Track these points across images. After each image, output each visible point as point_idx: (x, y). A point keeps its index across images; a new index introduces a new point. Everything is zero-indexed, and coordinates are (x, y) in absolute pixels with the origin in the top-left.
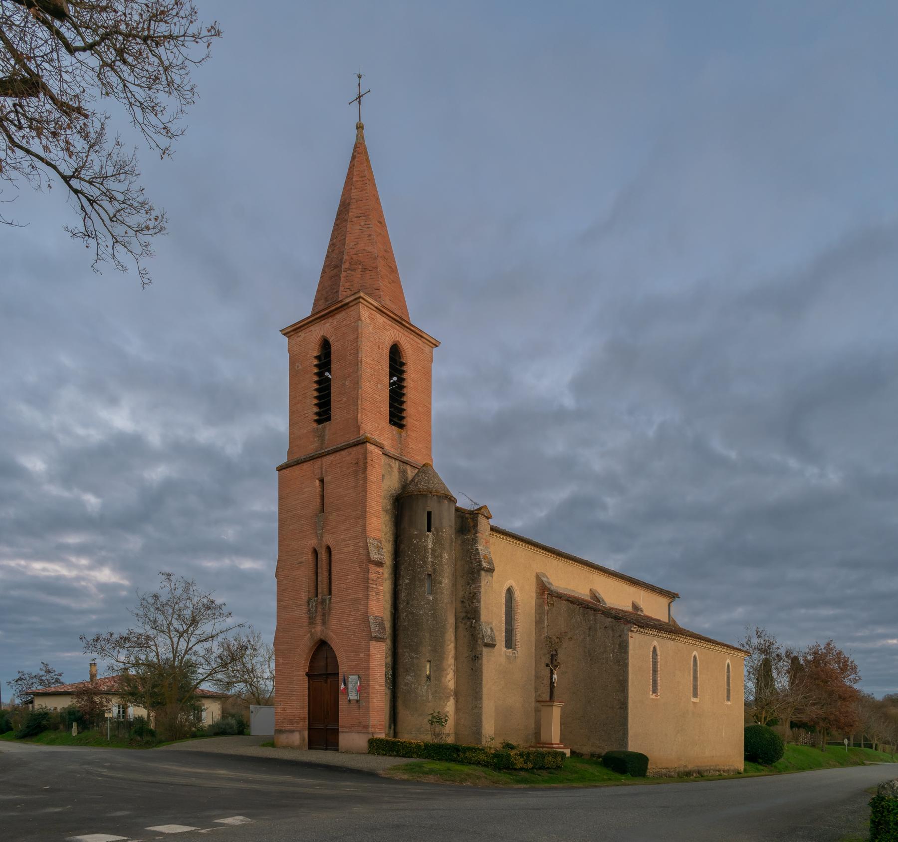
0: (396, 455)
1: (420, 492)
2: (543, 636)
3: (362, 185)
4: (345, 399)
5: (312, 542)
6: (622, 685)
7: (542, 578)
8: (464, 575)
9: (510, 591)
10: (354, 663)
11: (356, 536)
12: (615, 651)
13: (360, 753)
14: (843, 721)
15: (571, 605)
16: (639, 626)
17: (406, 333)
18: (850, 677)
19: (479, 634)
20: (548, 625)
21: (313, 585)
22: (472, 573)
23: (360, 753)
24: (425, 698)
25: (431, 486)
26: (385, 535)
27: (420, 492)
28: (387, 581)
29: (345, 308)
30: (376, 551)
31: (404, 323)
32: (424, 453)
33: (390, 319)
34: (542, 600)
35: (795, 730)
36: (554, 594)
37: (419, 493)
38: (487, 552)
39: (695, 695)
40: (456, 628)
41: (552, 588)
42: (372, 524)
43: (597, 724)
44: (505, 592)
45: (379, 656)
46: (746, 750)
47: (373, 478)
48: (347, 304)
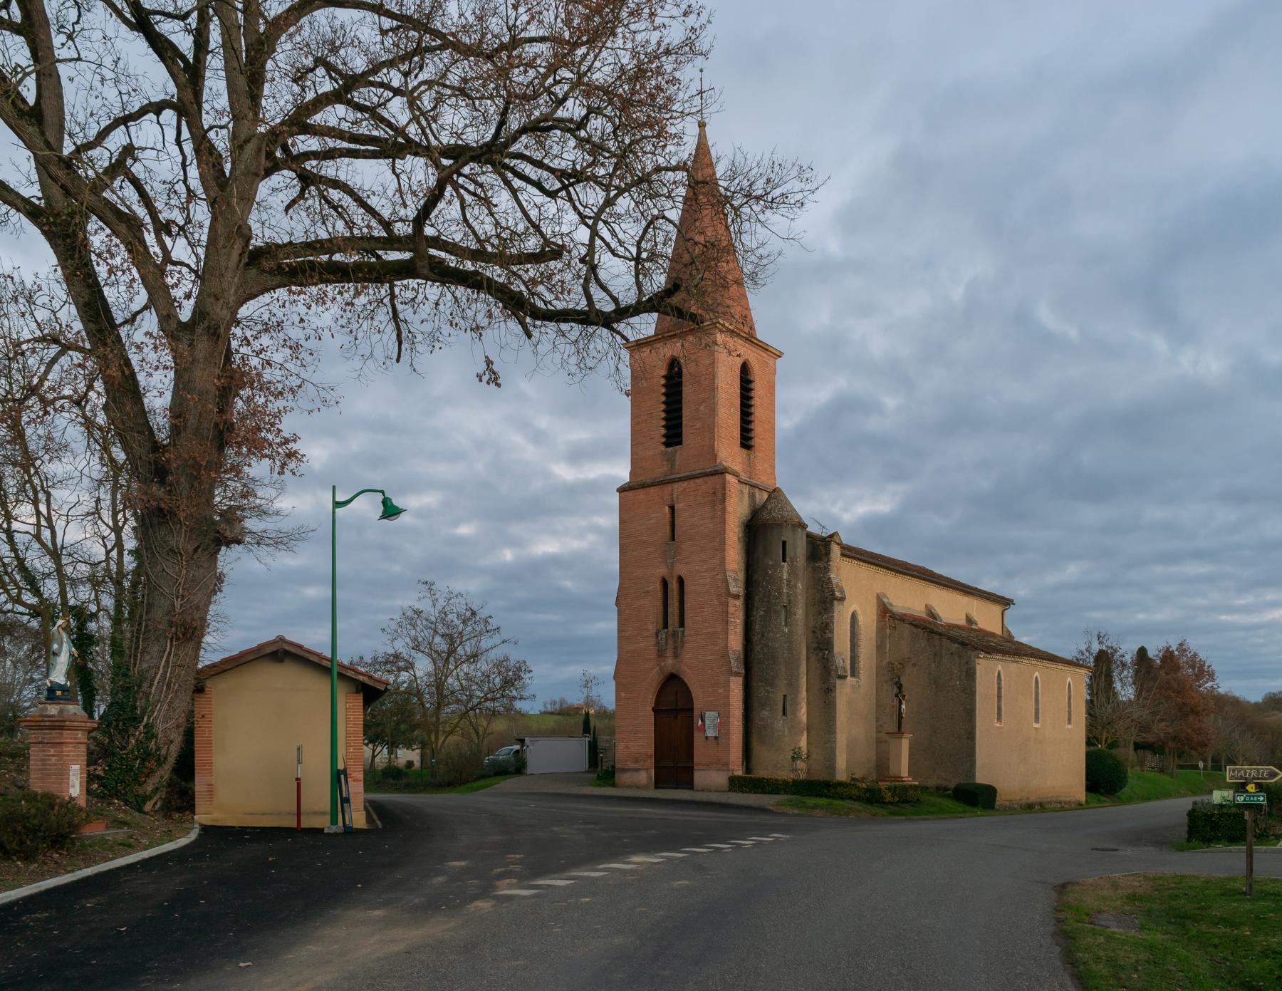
2: (885, 662)
4: (699, 425)
5: (662, 571)
6: (969, 713)
9: (854, 616)
10: (711, 699)
11: (714, 569)
14: (1196, 739)
16: (986, 652)
18: (1207, 685)
20: (890, 650)
21: (661, 615)
22: (825, 602)
25: (786, 514)
35: (1141, 752)
39: (1037, 720)
40: (808, 658)
41: (894, 610)
46: (1087, 779)
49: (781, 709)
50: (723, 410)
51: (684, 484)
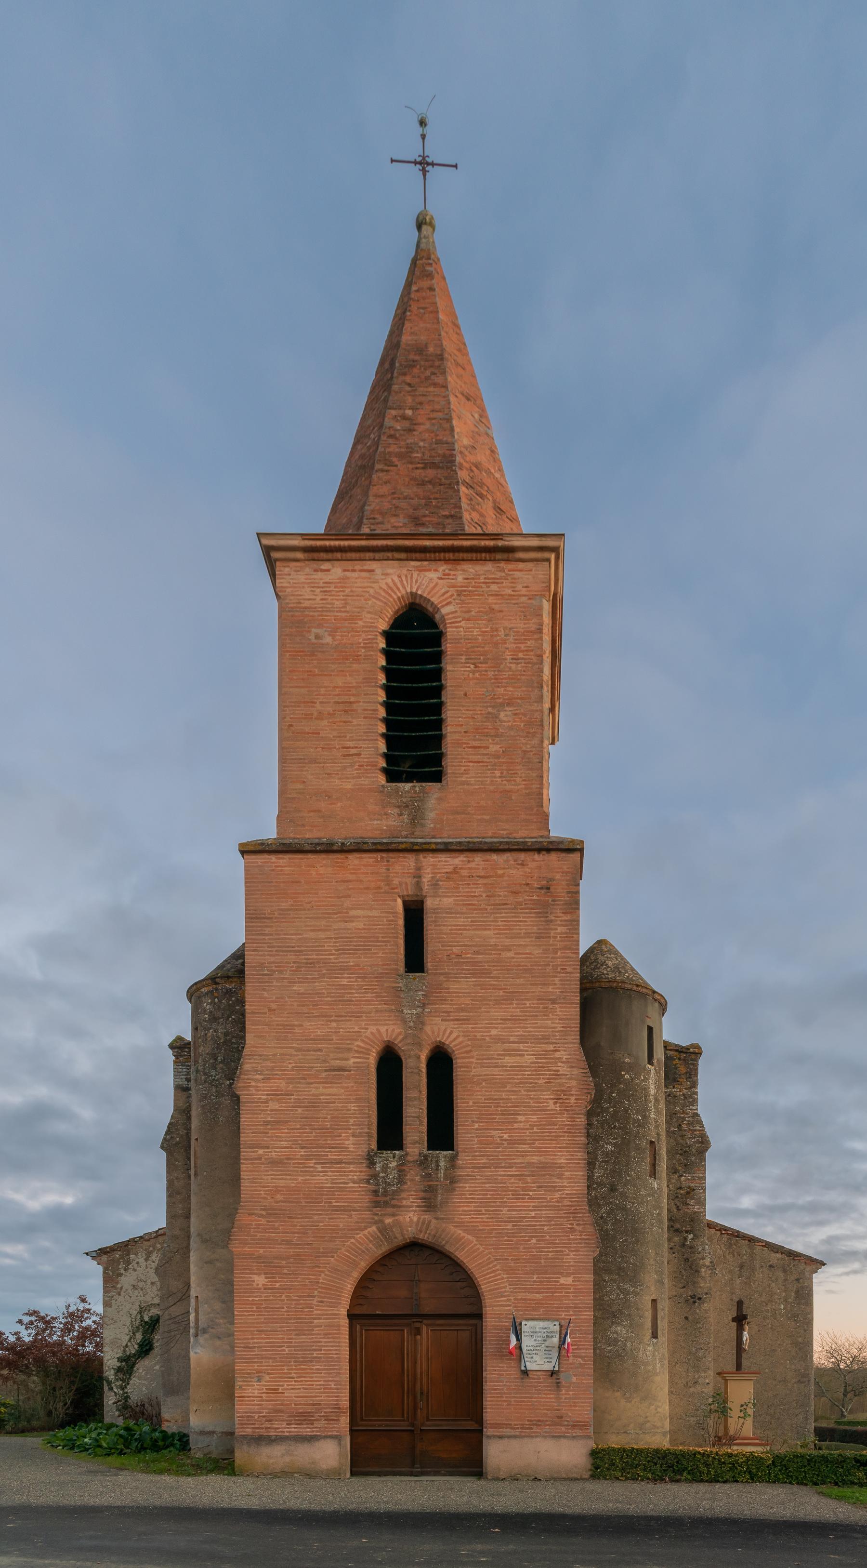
4: (494, 748)
12: (790, 1300)
24: (650, 1368)
29: (499, 556)
37: (635, 988)
49: (649, 1324)
51: (458, 860)
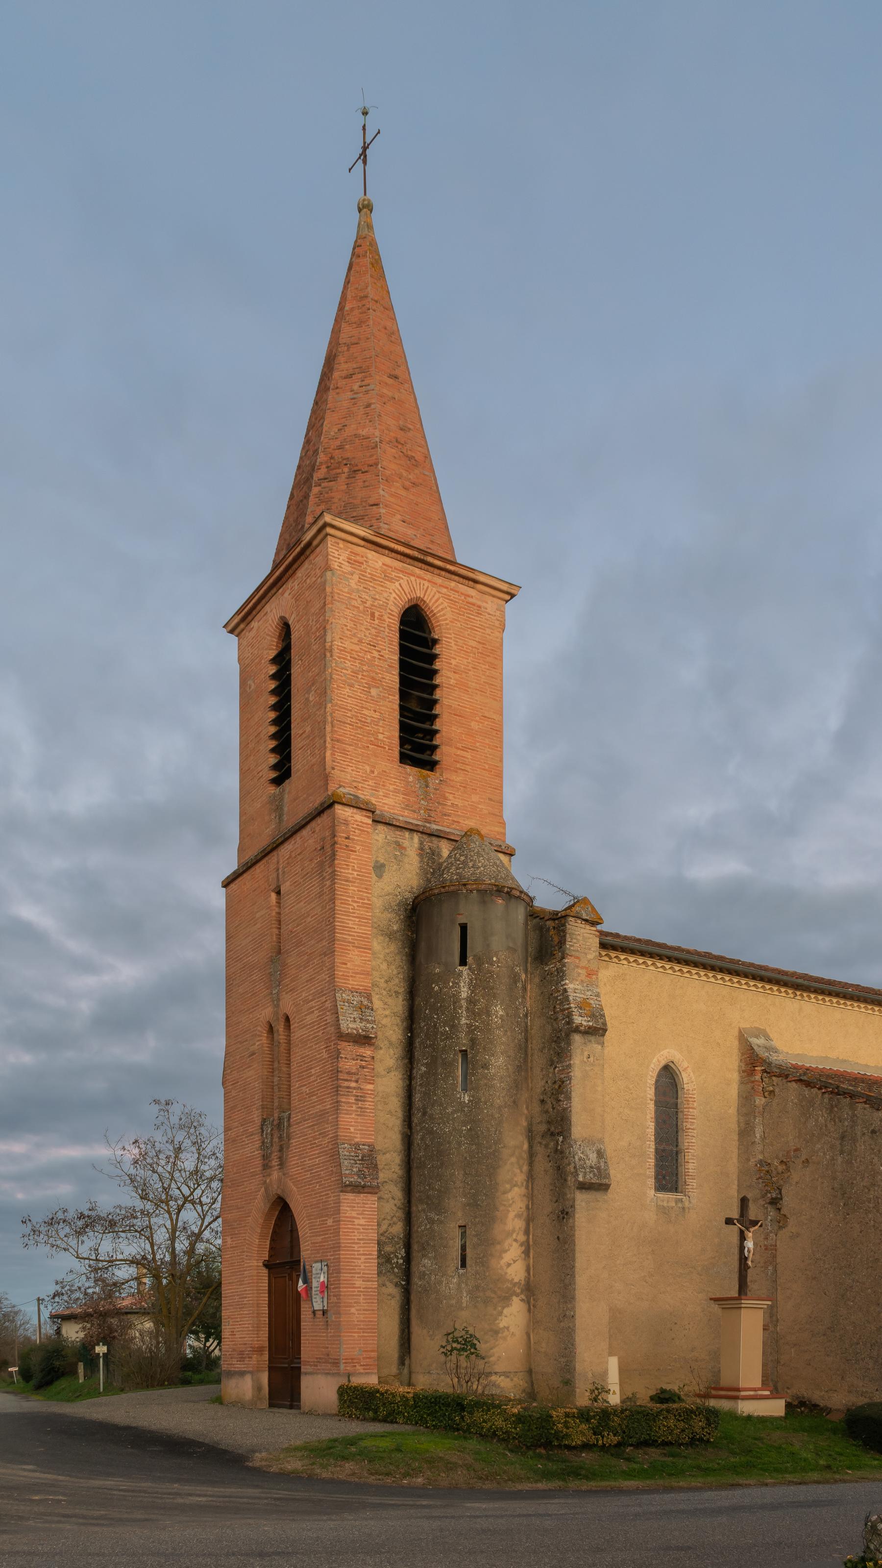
0: (411, 821)
1: (444, 887)
2: (752, 1162)
3: (361, 313)
5: (266, 1013)
7: (750, 1040)
8: (544, 1047)
13: (326, 1415)
15: (806, 1092)
17: (439, 580)
19: (569, 1164)
20: (763, 1138)
23: (326, 1415)
24: (453, 1302)
26: (386, 982)
27: (444, 887)
28: (393, 1074)
29: (308, 552)
30: (355, 1014)
31: (430, 559)
32: (486, 812)
33: (399, 557)
34: (749, 1086)
36: (775, 1070)
37: (443, 890)
38: (589, 993)
42: (349, 964)
43: (858, 1344)
44: (655, 1074)
45: (362, 1222)
47: (350, 871)
48: (309, 544)
50: (347, 691)
